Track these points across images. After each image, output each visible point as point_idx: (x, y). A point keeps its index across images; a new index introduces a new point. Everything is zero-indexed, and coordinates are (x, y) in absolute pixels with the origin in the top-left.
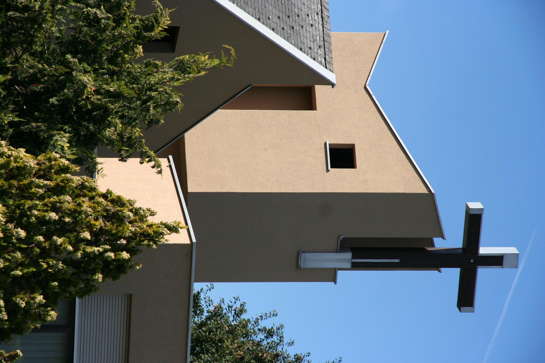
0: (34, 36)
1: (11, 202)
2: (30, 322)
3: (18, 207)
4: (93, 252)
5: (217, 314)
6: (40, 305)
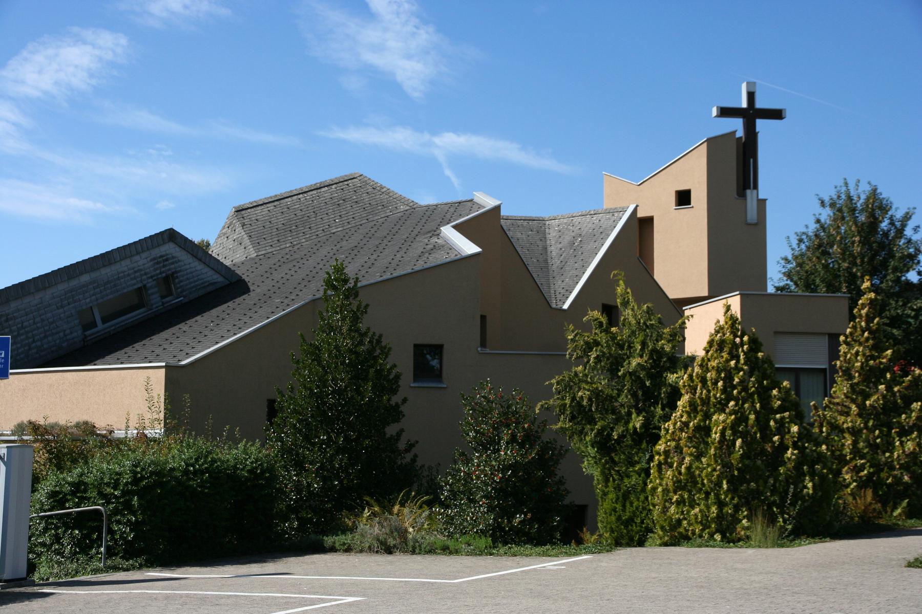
0: (607, 395)
1: (712, 410)
2: (791, 398)
3: (715, 406)
4: (744, 358)
5: (789, 275)
6: (779, 392)
